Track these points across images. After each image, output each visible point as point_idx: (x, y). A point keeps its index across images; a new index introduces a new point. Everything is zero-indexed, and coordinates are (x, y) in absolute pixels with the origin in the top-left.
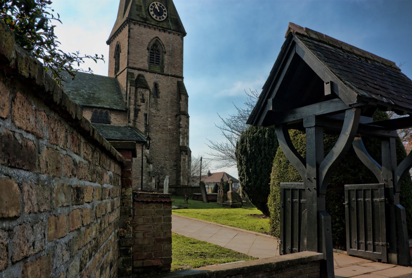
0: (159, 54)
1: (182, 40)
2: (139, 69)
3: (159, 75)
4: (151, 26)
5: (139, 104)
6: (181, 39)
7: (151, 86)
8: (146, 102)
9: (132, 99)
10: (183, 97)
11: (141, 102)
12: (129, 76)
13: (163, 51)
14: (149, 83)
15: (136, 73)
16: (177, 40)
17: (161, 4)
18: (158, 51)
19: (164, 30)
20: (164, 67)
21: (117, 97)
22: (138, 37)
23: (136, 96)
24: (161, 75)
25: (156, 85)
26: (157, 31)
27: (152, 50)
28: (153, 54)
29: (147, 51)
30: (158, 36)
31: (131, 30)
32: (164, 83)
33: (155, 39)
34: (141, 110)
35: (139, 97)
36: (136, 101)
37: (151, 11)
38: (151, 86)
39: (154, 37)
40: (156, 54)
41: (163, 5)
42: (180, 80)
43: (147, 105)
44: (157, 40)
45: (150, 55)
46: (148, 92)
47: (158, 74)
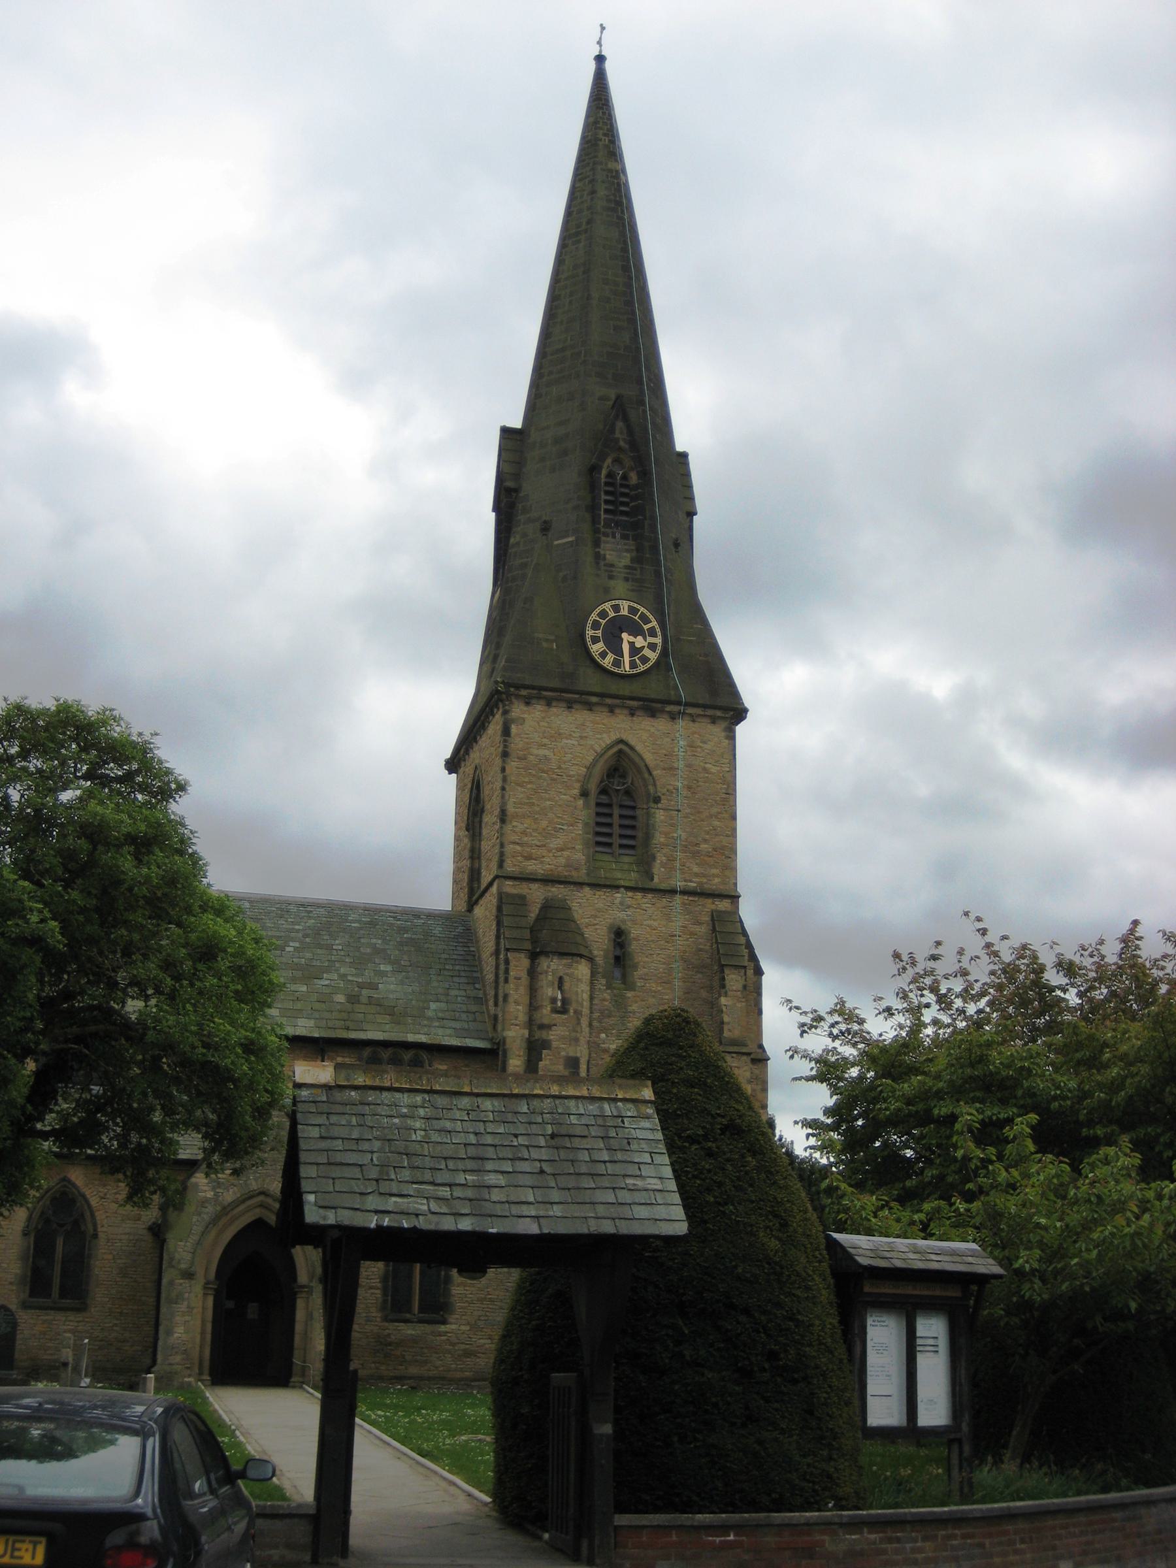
0: (634, 808)
1: (732, 737)
2: (547, 881)
3: (630, 894)
4: (594, 699)
5: (546, 1021)
6: (723, 734)
7: (598, 940)
8: (575, 1012)
9: (517, 1003)
10: (734, 980)
11: (555, 1011)
12: (506, 909)
13: (649, 794)
14: (588, 933)
15: (536, 894)
16: (705, 743)
17: (635, 605)
18: (628, 793)
19: (650, 707)
20: (654, 858)
21: (462, 993)
22: (542, 752)
23: (533, 990)
24: (639, 895)
25: (619, 936)
26: (621, 717)
27: (603, 791)
28: (606, 811)
29: (580, 802)
30: (624, 738)
31: (514, 729)
32: (656, 924)
33: (615, 749)
34: (555, 1044)
35: (549, 991)
36: (533, 1007)
37: (595, 640)
38: (598, 940)
39: (608, 742)
40: (621, 806)
41: (642, 609)
42: (723, 905)
43: (579, 1023)
44: (620, 751)
45: (598, 814)
46: (583, 970)
47: (628, 888)
